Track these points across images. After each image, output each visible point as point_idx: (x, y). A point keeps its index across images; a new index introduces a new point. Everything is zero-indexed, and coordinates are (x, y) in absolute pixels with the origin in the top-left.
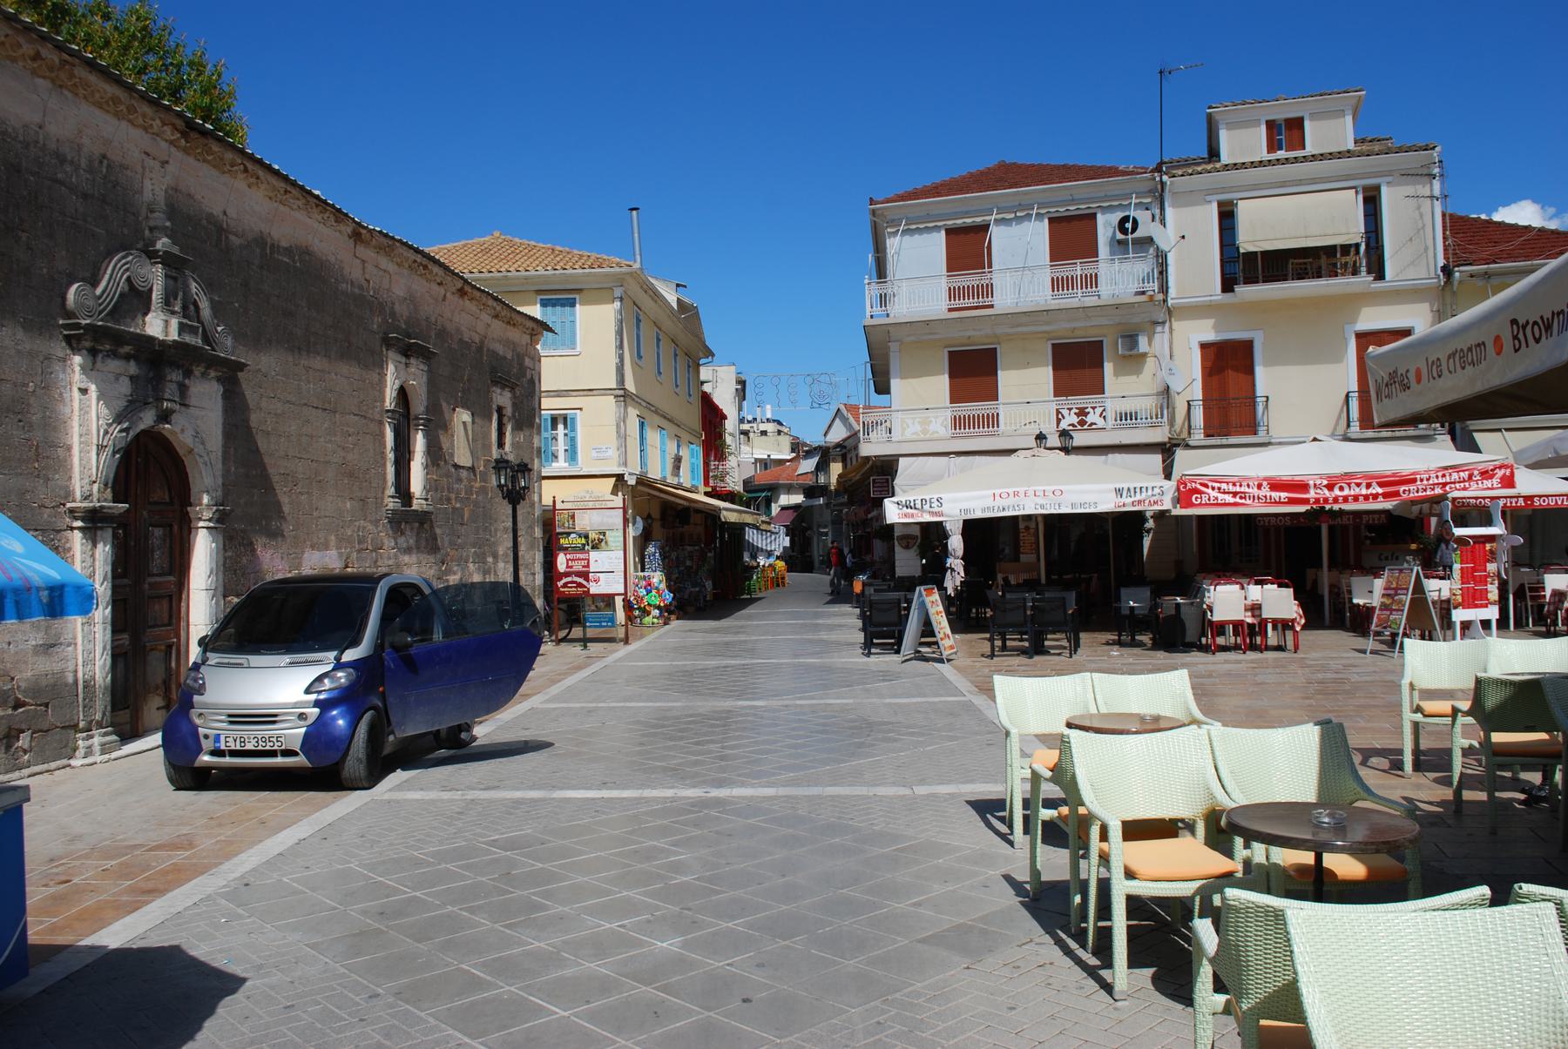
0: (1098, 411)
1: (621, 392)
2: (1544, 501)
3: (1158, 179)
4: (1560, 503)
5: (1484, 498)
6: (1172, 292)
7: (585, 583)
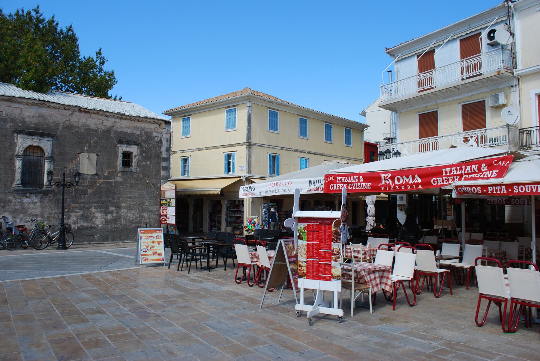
0: (474, 138)
1: (248, 144)
2: (522, 189)
3: (506, 5)
4: (534, 191)
5: (476, 186)
6: (519, 67)
7: (166, 219)
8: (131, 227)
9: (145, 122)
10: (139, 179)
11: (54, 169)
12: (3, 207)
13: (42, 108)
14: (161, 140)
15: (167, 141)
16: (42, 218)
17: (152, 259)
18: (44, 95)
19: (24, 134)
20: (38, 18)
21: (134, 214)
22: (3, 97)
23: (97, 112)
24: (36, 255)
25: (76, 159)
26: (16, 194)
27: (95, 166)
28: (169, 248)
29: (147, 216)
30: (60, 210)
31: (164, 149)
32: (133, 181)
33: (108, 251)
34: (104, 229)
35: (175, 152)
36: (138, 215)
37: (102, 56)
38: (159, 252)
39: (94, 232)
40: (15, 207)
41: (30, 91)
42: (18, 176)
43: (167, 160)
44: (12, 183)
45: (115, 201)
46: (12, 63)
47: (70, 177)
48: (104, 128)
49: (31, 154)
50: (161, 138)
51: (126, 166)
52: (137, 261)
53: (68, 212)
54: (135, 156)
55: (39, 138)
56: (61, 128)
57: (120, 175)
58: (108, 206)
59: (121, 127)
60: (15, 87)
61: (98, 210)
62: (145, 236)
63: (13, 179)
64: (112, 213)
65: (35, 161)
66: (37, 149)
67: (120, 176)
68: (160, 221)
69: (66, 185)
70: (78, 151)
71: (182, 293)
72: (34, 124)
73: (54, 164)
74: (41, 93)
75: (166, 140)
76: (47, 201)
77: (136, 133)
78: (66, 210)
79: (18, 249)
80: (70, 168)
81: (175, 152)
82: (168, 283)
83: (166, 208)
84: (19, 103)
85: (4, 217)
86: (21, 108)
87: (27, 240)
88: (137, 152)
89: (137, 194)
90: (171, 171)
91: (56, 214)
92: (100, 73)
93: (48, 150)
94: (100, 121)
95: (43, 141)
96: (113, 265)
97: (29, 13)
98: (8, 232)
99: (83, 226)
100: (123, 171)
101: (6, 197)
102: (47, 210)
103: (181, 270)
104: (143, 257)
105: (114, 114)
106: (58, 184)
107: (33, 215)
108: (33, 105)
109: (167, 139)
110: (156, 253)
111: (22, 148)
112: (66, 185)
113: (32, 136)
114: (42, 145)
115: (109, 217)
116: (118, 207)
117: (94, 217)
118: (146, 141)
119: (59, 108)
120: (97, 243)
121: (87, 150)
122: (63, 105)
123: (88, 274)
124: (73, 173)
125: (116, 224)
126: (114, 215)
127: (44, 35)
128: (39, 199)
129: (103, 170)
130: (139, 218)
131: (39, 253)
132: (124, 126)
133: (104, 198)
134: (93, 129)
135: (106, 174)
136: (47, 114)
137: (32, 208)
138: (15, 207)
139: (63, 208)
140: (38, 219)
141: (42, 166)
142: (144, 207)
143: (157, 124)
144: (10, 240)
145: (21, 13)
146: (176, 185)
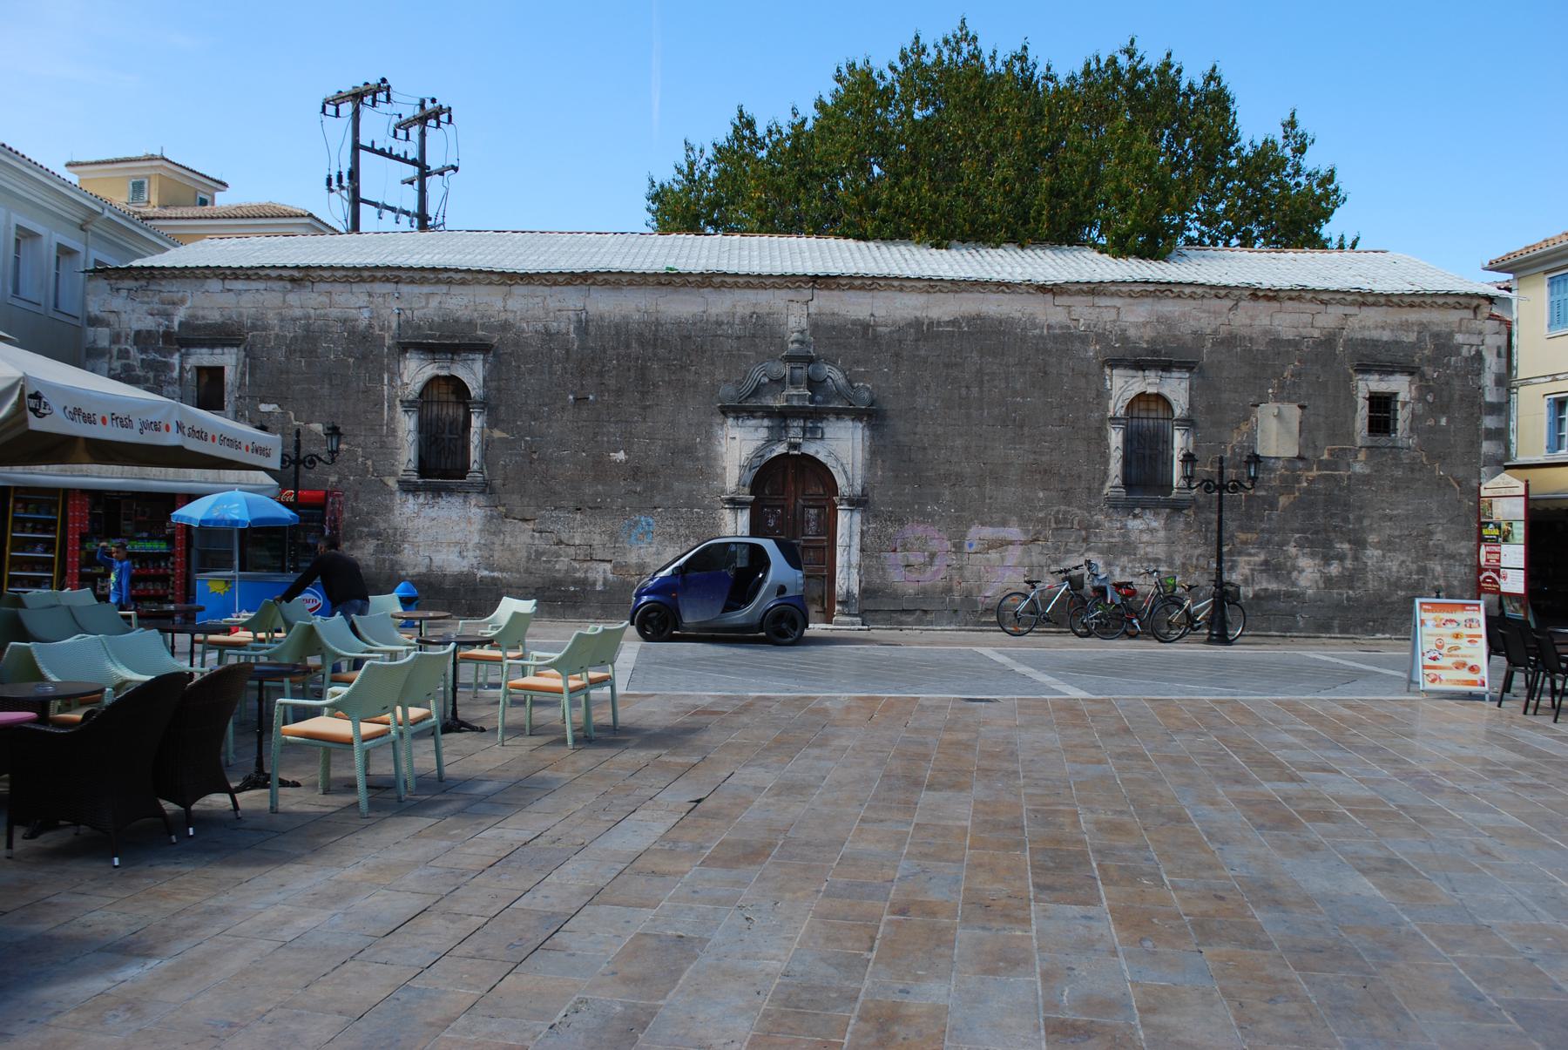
7: (1497, 579)
8: (1395, 598)
9: (1432, 306)
10: (1417, 467)
11: (1196, 447)
12: (1085, 540)
13: (1163, 301)
14: (1479, 353)
15: (1499, 355)
16: (1169, 567)
17: (1451, 679)
18: (1163, 265)
19: (1125, 367)
20: (1133, 70)
21: (1403, 562)
22: (1079, 286)
23: (1300, 294)
24: (1161, 653)
25: (1247, 419)
26: (1111, 510)
27: (1297, 436)
28: (1503, 655)
29: (1439, 568)
30: (1213, 549)
31: (1488, 379)
32: (1399, 473)
33: (1333, 656)
34: (1321, 601)
35: (1527, 382)
36: (1414, 567)
37: (1299, 130)
38: (1471, 662)
39: (1296, 606)
40: (1111, 540)
41: (1130, 259)
42: (1115, 467)
43: (1502, 409)
44: (1103, 483)
45: (1351, 526)
46: (1086, 197)
47: (1236, 467)
48: (1316, 334)
49: (1143, 414)
50: (1481, 348)
51: (1378, 432)
52: (1411, 682)
53: (1231, 553)
54: (1405, 404)
55: (1160, 373)
56: (1210, 345)
57: (1362, 456)
58: (1331, 541)
59: (1363, 328)
60: (1095, 254)
61: (1305, 550)
62: (1435, 619)
63: (1105, 474)
64: (1341, 558)
65: (1152, 429)
66: (1157, 402)
67: (1363, 459)
68: (1479, 583)
69: (1226, 487)
70: (1252, 400)
71: (1529, 760)
72: (1147, 342)
73: (1195, 434)
74: (1155, 260)
75: (1495, 351)
76: (1182, 526)
77: (1405, 339)
78: (1225, 549)
79: (1119, 637)
80: (1234, 443)
81: (1527, 382)
82: (1493, 737)
83: (1496, 549)
84: (1113, 295)
85: (1088, 562)
86: (1118, 305)
87: (1137, 618)
88: (1410, 391)
89: (1410, 507)
90: (1513, 438)
91: (1201, 559)
92: (1294, 177)
93: (1181, 402)
94: (1307, 318)
95: (1168, 380)
96: (1348, 686)
97: (1113, 61)
98: (1098, 597)
99: (1266, 590)
100: (1372, 447)
101: (1092, 517)
102: (1181, 549)
103: (1535, 714)
104: (1427, 671)
105: (1341, 296)
106: (1207, 485)
107: (1149, 560)
108: (1142, 295)
109: (1499, 348)
110: (1464, 665)
111: (1123, 401)
112: (1226, 487)
113: (1144, 370)
114: (1166, 391)
115: (1334, 569)
116: (1359, 544)
117: (1294, 568)
118: (1433, 361)
119: (1203, 296)
120: (1303, 634)
121: (1275, 396)
122: (1212, 287)
123: (1289, 700)
124: (1241, 456)
125: (1351, 588)
126: (1348, 564)
127: (1152, 108)
128: (1163, 522)
129: (1316, 446)
130: (1418, 573)
131: (1167, 648)
132: (1370, 324)
133: (1320, 520)
134: (1289, 340)
135: (1325, 456)
136: (1177, 314)
137: (1148, 543)
138: (1111, 540)
139: (1220, 545)
140: (1161, 569)
141: (1168, 442)
142: (1431, 543)
143: (1466, 308)
144: (1102, 615)
145: (1093, 66)
146: (1527, 481)
